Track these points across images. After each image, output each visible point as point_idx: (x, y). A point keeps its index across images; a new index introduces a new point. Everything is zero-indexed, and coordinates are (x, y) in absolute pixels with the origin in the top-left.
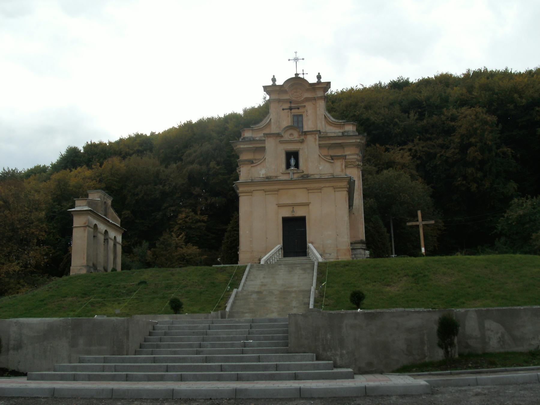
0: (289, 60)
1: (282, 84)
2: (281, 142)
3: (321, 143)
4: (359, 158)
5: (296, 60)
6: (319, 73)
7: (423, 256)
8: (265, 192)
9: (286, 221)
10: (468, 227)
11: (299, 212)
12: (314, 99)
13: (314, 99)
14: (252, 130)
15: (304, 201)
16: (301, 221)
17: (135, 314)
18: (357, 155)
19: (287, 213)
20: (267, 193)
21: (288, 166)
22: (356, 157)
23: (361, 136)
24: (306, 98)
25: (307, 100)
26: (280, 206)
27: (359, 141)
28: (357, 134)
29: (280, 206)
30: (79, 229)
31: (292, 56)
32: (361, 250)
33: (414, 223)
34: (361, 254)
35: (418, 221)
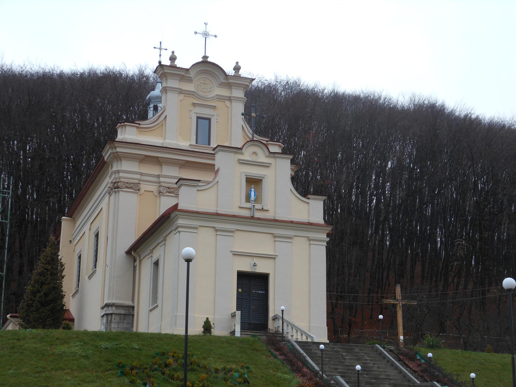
0: (196, 33)
1: (188, 66)
2: (242, 162)
5: (206, 35)
6: (237, 63)
8: (275, 237)
9: (242, 276)
10: (460, 310)
11: (262, 268)
12: (230, 99)
13: (230, 99)
14: (137, 127)
15: (271, 252)
17: (502, 285)
19: (246, 266)
21: (248, 199)
24: (217, 95)
25: (220, 98)
26: (236, 254)
29: (236, 254)
30: (302, 238)
31: (201, 29)
33: (392, 302)
35: (395, 298)
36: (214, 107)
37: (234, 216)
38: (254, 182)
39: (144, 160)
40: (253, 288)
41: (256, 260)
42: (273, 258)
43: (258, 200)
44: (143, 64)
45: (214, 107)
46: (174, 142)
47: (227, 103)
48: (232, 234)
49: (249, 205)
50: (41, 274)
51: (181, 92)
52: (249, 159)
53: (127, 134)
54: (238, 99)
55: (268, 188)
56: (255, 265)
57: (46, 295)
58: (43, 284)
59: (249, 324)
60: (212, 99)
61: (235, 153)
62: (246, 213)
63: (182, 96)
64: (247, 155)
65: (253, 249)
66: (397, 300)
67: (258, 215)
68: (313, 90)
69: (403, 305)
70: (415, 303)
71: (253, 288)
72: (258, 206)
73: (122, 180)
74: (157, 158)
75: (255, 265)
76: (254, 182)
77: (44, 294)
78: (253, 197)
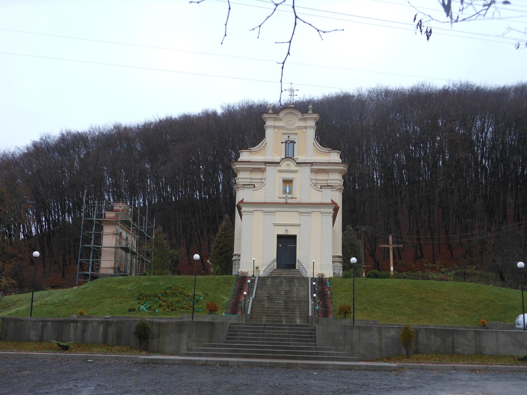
2: (280, 171)
3: (386, 246)
4: (342, 183)
7: (392, 277)
8: (300, 213)
9: (280, 238)
11: (291, 232)
12: (305, 127)
13: (305, 127)
16: (294, 238)
18: (340, 180)
19: (282, 232)
20: (301, 214)
21: (285, 192)
22: (339, 182)
23: (344, 165)
25: (300, 128)
26: (276, 225)
27: (342, 168)
28: (340, 161)
29: (276, 225)
32: (338, 263)
33: (386, 246)
34: (338, 266)
36: (296, 134)
37: (274, 203)
38: (288, 182)
39: (253, 170)
40: (287, 244)
41: (287, 228)
42: (299, 225)
43: (290, 193)
44: (359, 86)
45: (296, 134)
46: (272, 158)
47: (304, 130)
48: (273, 214)
49: (284, 196)
50: (220, 237)
51: (275, 127)
52: (285, 169)
53: (244, 156)
54: (310, 127)
55: (296, 186)
56: (287, 230)
57: (221, 249)
58: (220, 242)
59: (286, 264)
60: (295, 129)
61: (276, 166)
62: (283, 201)
63: (276, 130)
64: (284, 166)
65: (287, 221)
66: (389, 245)
67: (289, 201)
68: (504, 88)
69: (393, 248)
70: (402, 246)
71: (287, 244)
72: (289, 196)
73: (240, 183)
74: (260, 168)
75: (287, 230)
76: (288, 182)
77: (221, 248)
78: (288, 191)
